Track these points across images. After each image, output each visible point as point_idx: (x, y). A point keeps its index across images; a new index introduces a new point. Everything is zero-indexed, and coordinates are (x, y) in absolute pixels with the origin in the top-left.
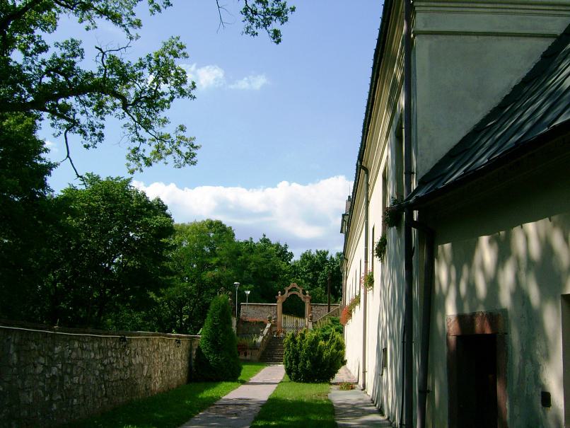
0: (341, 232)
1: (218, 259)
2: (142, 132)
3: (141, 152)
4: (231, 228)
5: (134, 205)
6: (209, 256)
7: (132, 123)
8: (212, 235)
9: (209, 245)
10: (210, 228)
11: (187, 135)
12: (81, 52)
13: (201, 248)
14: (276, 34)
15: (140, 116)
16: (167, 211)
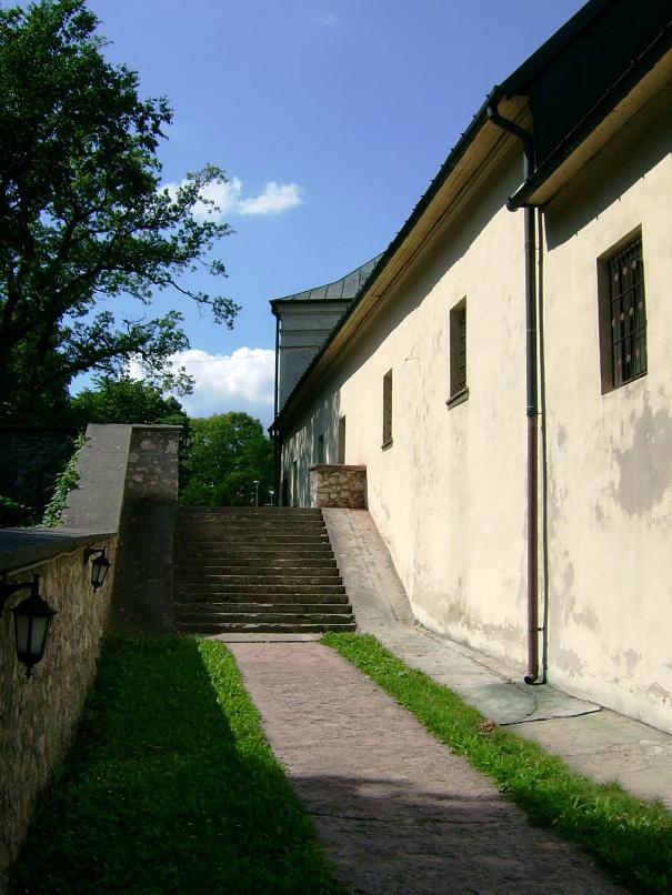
0: (343, 421)
1: (242, 458)
2: (156, 371)
3: (155, 385)
4: (258, 420)
5: (149, 407)
6: (235, 455)
7: (148, 365)
8: (237, 429)
9: (234, 442)
10: (233, 422)
11: (187, 373)
12: (112, 320)
13: (224, 446)
14: (230, 324)
15: (154, 361)
16: (182, 410)
